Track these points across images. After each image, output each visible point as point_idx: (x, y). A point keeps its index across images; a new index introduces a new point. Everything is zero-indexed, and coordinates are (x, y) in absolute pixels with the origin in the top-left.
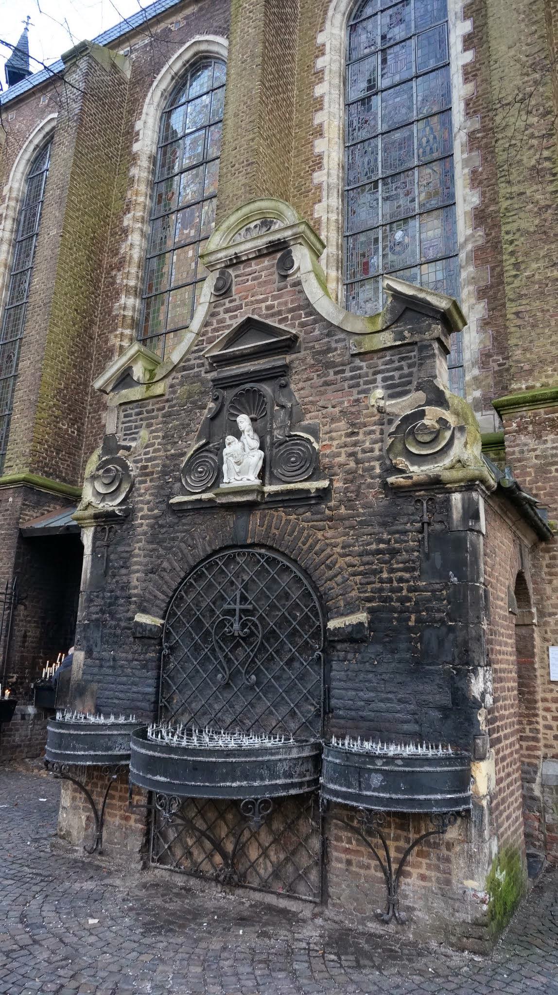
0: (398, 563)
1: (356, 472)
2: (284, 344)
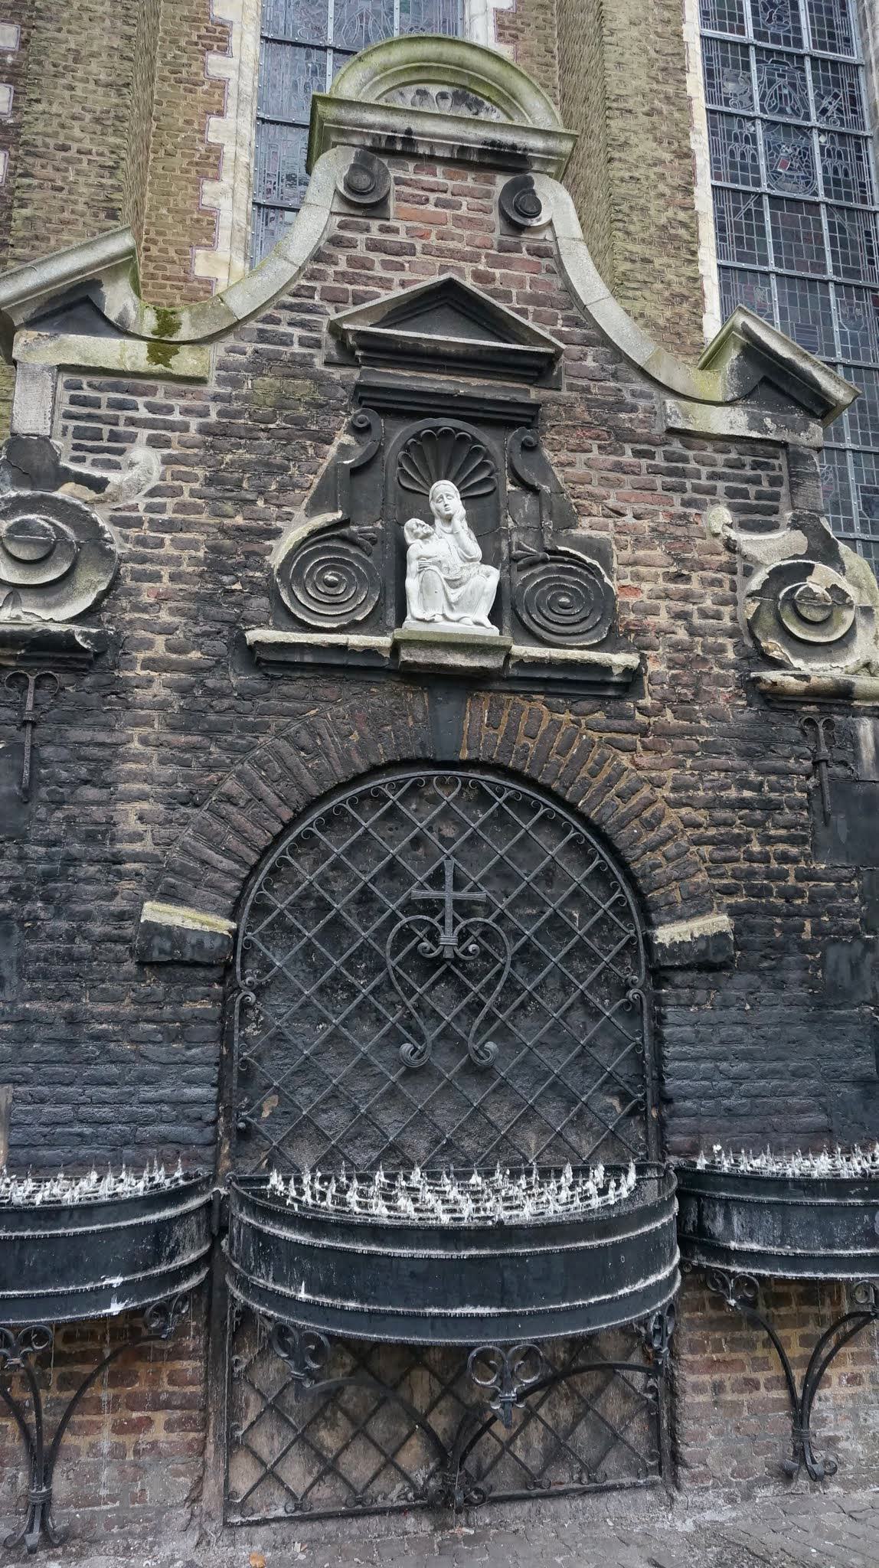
0: (776, 826)
1: (691, 650)
2: (534, 362)
